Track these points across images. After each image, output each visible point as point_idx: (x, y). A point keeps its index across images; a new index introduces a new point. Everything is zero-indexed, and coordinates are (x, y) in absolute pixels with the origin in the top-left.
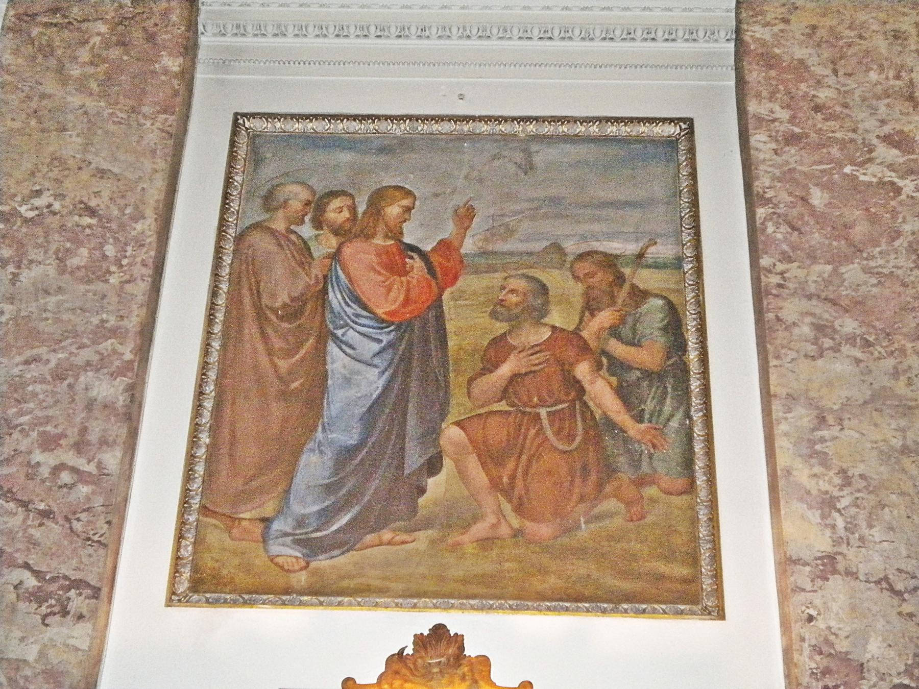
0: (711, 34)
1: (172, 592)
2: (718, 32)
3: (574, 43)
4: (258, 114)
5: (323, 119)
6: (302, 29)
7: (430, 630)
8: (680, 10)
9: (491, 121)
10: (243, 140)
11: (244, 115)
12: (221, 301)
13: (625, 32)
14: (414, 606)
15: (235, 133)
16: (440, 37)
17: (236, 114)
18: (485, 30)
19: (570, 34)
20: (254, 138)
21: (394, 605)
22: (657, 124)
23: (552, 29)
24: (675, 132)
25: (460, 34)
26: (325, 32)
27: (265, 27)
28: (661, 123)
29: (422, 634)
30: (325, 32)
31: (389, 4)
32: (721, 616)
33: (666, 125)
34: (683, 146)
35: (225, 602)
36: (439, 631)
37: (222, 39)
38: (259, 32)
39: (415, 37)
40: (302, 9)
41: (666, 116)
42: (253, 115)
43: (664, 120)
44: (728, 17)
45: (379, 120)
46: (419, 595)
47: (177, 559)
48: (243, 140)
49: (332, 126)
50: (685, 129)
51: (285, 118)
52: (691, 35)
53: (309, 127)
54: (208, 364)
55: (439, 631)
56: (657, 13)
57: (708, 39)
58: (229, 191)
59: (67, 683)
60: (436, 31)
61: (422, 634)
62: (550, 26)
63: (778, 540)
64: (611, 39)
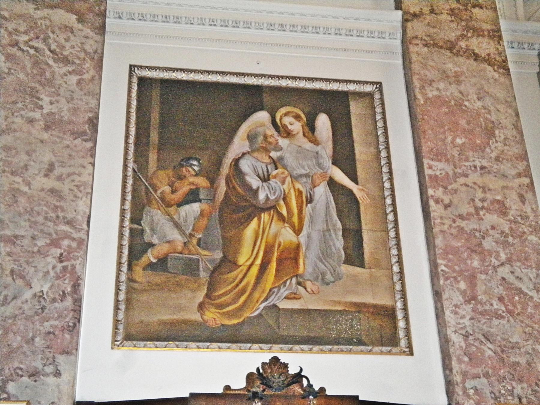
1: (114, 340)
2: (331, 29)
3: (159, 24)
4: (319, 79)
6: (155, 17)
7: (270, 360)
13: (211, 21)
14: (291, 350)
15: (131, 75)
17: (131, 66)
18: (328, 29)
19: (180, 20)
20: (142, 80)
21: (133, 346)
25: (529, 47)
26: (180, 20)
27: (205, 20)
30: (227, 24)
31: (217, 7)
32: (411, 353)
34: (377, 96)
35: (342, 351)
36: (275, 360)
38: (213, 23)
39: (289, 31)
41: (375, 81)
42: (141, 67)
43: (367, 83)
45: (141, 68)
47: (116, 322)
48: (135, 80)
51: (300, 79)
54: (124, 210)
55: (275, 360)
60: (112, 14)
63: (224, 305)
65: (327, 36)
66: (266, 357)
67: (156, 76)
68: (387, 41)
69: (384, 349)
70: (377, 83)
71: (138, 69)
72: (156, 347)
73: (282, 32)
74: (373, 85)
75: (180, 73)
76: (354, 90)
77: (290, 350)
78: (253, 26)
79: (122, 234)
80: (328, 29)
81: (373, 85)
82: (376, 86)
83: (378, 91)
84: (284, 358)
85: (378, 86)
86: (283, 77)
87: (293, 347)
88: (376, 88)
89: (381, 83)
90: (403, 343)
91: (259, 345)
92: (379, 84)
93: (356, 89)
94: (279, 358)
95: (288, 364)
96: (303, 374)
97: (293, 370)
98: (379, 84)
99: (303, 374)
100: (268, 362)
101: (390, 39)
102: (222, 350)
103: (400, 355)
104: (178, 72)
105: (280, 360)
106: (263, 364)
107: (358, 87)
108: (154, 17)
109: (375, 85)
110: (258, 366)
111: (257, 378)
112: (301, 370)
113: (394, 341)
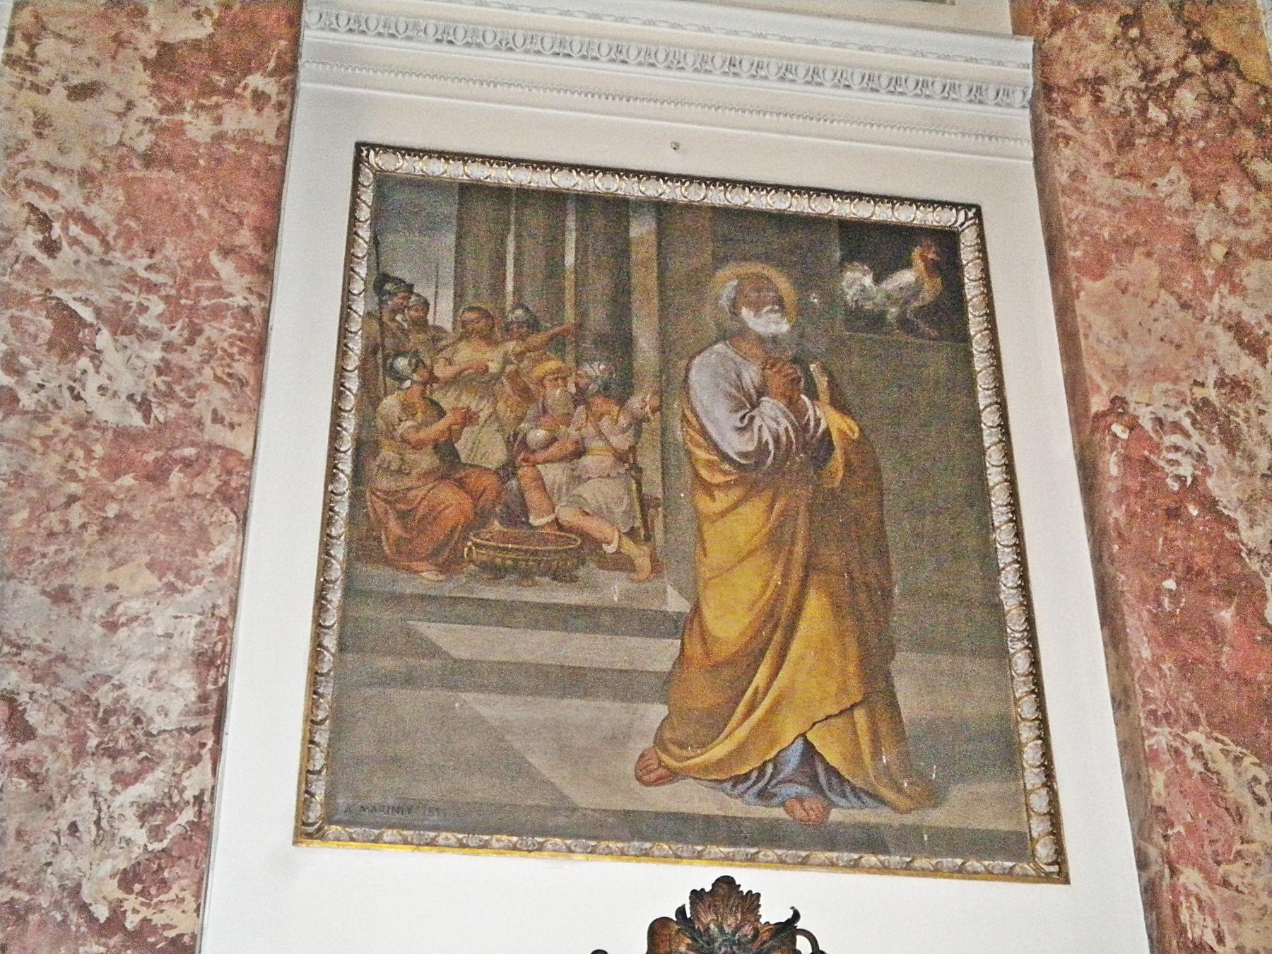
0: (1003, 94)
5: (911, 205)
8: (612, 18)
9: (409, 155)
10: (367, 177)
11: (371, 146)
12: (350, 403)
15: (357, 171)
16: (438, 40)
17: (359, 146)
20: (382, 180)
22: (768, 192)
23: (514, 36)
24: (956, 221)
26: (480, 40)
28: (773, 191)
29: (703, 890)
32: (1063, 877)
33: (652, 181)
34: (968, 238)
37: (333, 35)
39: (691, 69)
40: (863, 53)
42: (386, 148)
44: (1026, 75)
46: (545, 833)
48: (367, 177)
49: (406, 164)
50: (971, 219)
52: (977, 94)
53: (417, 168)
55: (726, 883)
56: (825, 48)
57: (919, 92)
58: (352, 251)
59: (1248, 951)
61: (703, 890)
62: (653, 49)
64: (451, 42)
65: (445, 47)
66: (704, 876)
67: (935, 224)
68: (990, 111)
69: (948, 862)
70: (968, 207)
71: (376, 154)
72: (352, 840)
73: (732, 80)
74: (958, 211)
75: (481, 166)
76: (868, 219)
77: (750, 860)
78: (401, 31)
79: (328, 554)
80: (925, 84)
81: (958, 211)
82: (966, 214)
83: (972, 225)
84: (747, 879)
85: (970, 214)
86: (902, 200)
87: (383, 832)
88: (967, 219)
89: (978, 208)
90: (1044, 851)
91: (776, 851)
92: (974, 210)
93: (831, 211)
94: (737, 883)
95: (758, 895)
96: (800, 925)
97: (772, 913)
98: (974, 210)
99: (799, 925)
100: (708, 888)
101: (997, 105)
102: (467, 850)
103: (1038, 882)
104: (432, 161)
105: (739, 886)
106: (696, 895)
107: (580, 181)
108: (732, 64)
109: (962, 213)
110: (680, 905)
111: (678, 931)
112: (796, 916)
113: (1018, 846)
